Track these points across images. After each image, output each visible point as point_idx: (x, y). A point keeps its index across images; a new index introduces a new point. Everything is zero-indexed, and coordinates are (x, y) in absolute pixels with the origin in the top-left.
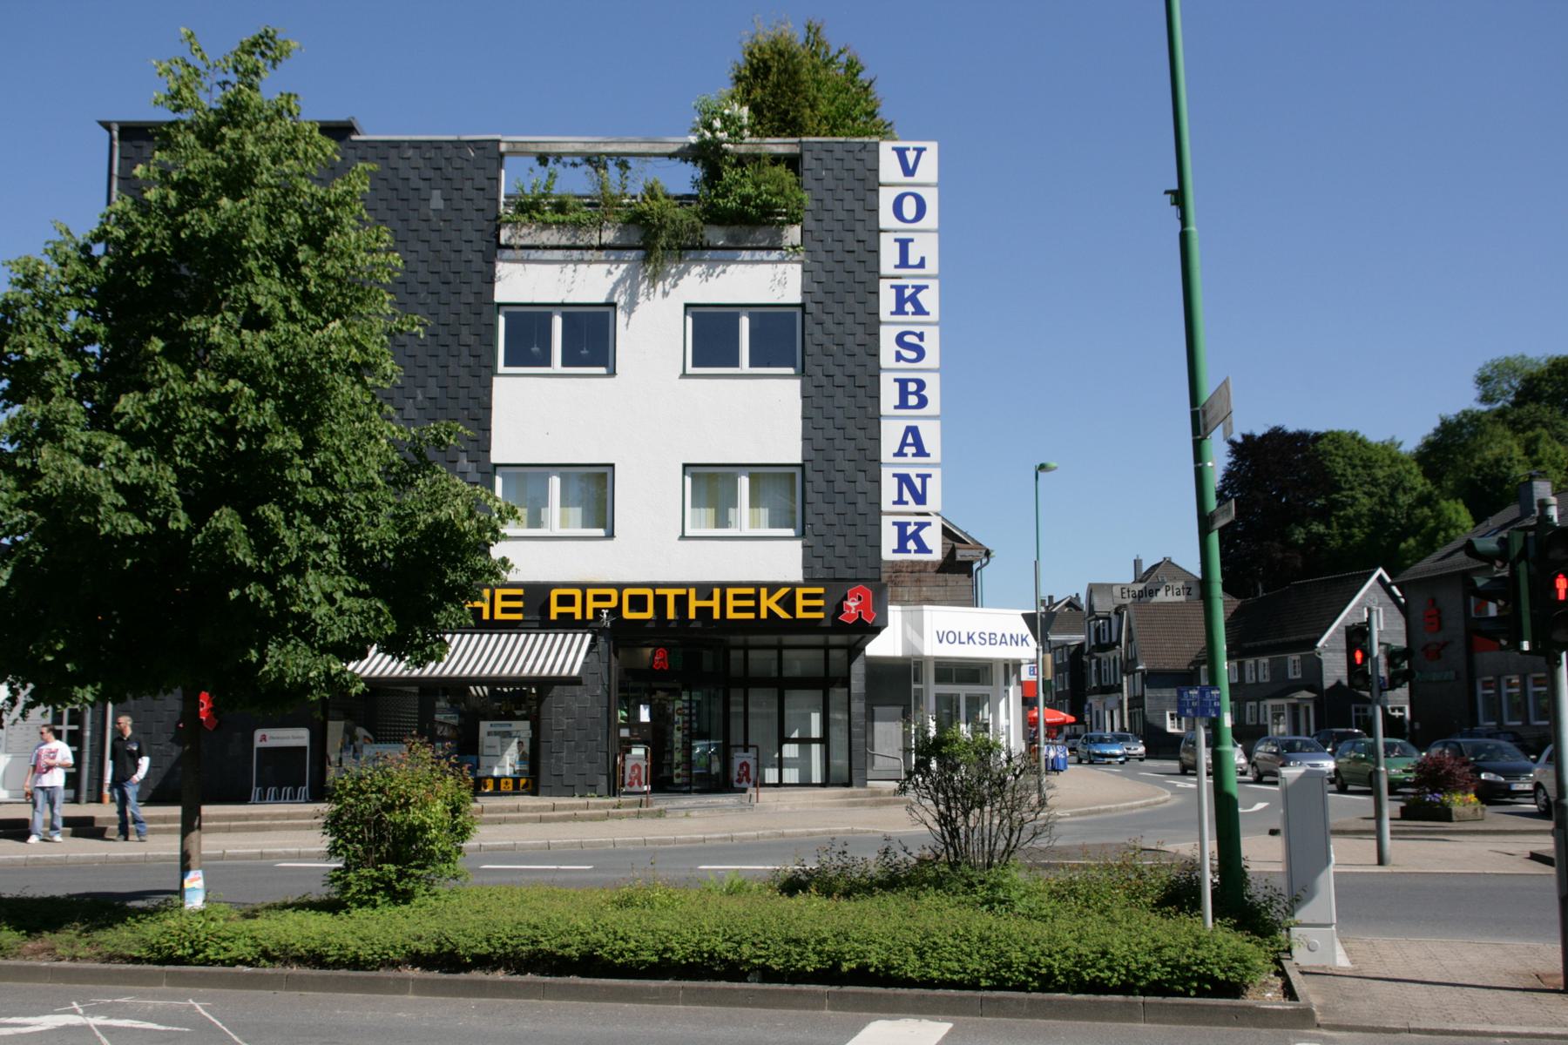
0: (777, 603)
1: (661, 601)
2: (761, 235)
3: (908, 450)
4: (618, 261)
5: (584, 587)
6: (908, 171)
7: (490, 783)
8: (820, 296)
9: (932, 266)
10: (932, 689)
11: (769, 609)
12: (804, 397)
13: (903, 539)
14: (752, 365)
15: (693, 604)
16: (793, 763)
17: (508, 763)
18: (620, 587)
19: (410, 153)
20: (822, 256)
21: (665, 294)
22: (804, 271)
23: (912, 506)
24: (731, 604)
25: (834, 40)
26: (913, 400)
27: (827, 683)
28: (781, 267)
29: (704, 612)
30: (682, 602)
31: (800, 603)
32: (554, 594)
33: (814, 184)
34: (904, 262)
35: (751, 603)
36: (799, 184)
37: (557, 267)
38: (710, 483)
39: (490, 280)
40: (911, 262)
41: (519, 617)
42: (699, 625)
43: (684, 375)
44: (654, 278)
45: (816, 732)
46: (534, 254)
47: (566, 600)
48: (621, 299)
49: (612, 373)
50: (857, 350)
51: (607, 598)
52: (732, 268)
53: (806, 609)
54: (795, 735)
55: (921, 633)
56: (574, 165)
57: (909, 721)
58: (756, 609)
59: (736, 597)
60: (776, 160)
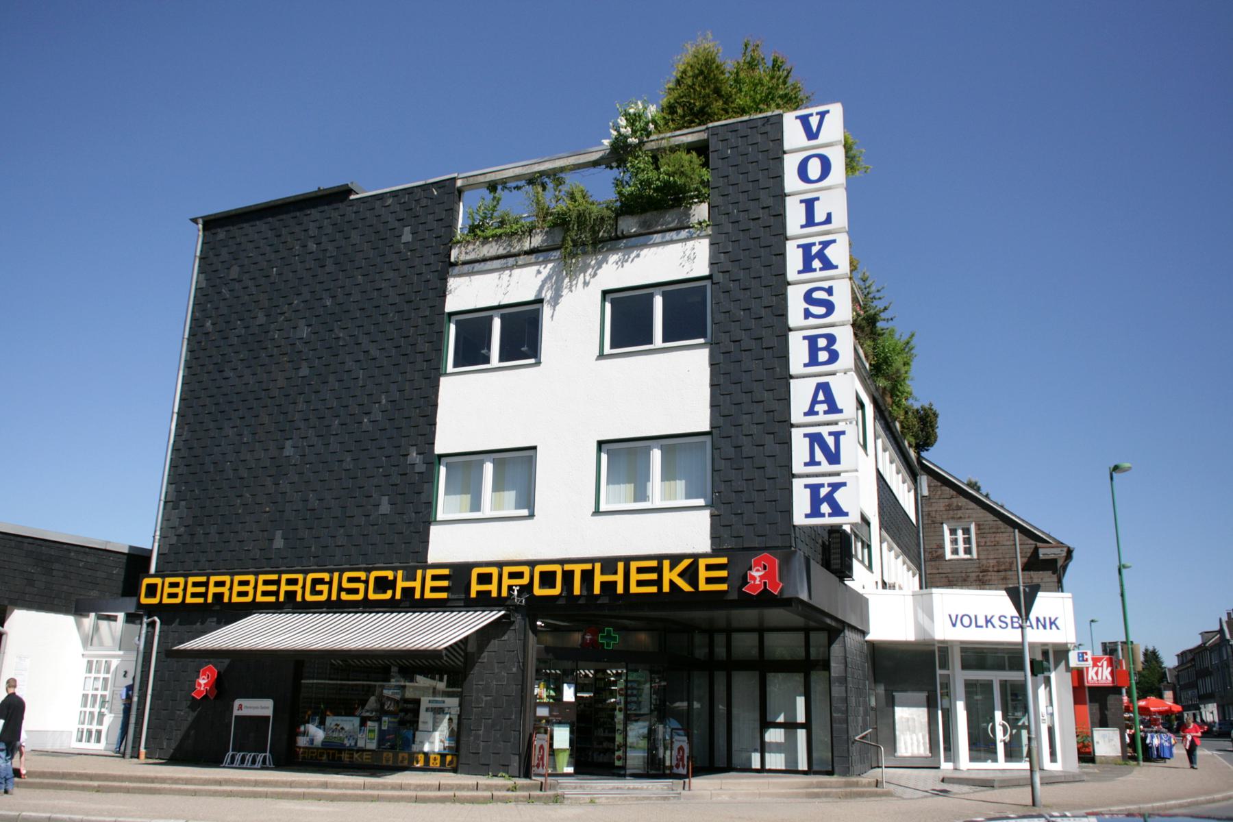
0: (681, 575)
1: (568, 576)
2: (670, 218)
3: (818, 408)
4: (545, 262)
5: (500, 565)
6: (811, 135)
7: (421, 757)
8: (728, 266)
9: (841, 219)
10: (960, 677)
11: (672, 583)
12: (712, 365)
13: (816, 502)
14: (664, 341)
15: (598, 578)
16: (778, 748)
17: (436, 741)
18: (532, 564)
19: (390, 201)
20: (729, 228)
21: (586, 284)
22: (711, 244)
23: (825, 467)
24: (634, 577)
25: (767, 55)
26: (823, 356)
27: (808, 667)
28: (690, 244)
29: (608, 587)
30: (587, 576)
31: (703, 574)
32: (475, 572)
33: (720, 163)
34: (810, 221)
35: (654, 576)
36: (706, 164)
37: (496, 275)
38: (623, 456)
39: (443, 295)
40: (817, 220)
41: (444, 595)
42: (605, 600)
43: (601, 356)
44: (572, 275)
45: (801, 718)
46: (477, 267)
47: (485, 579)
48: (547, 295)
49: (538, 363)
50: (763, 312)
51: (520, 575)
52: (645, 252)
53: (709, 581)
54: (781, 719)
55: (931, 616)
56: (518, 188)
57: (936, 707)
58: (658, 583)
59: (640, 570)
60: (690, 148)
